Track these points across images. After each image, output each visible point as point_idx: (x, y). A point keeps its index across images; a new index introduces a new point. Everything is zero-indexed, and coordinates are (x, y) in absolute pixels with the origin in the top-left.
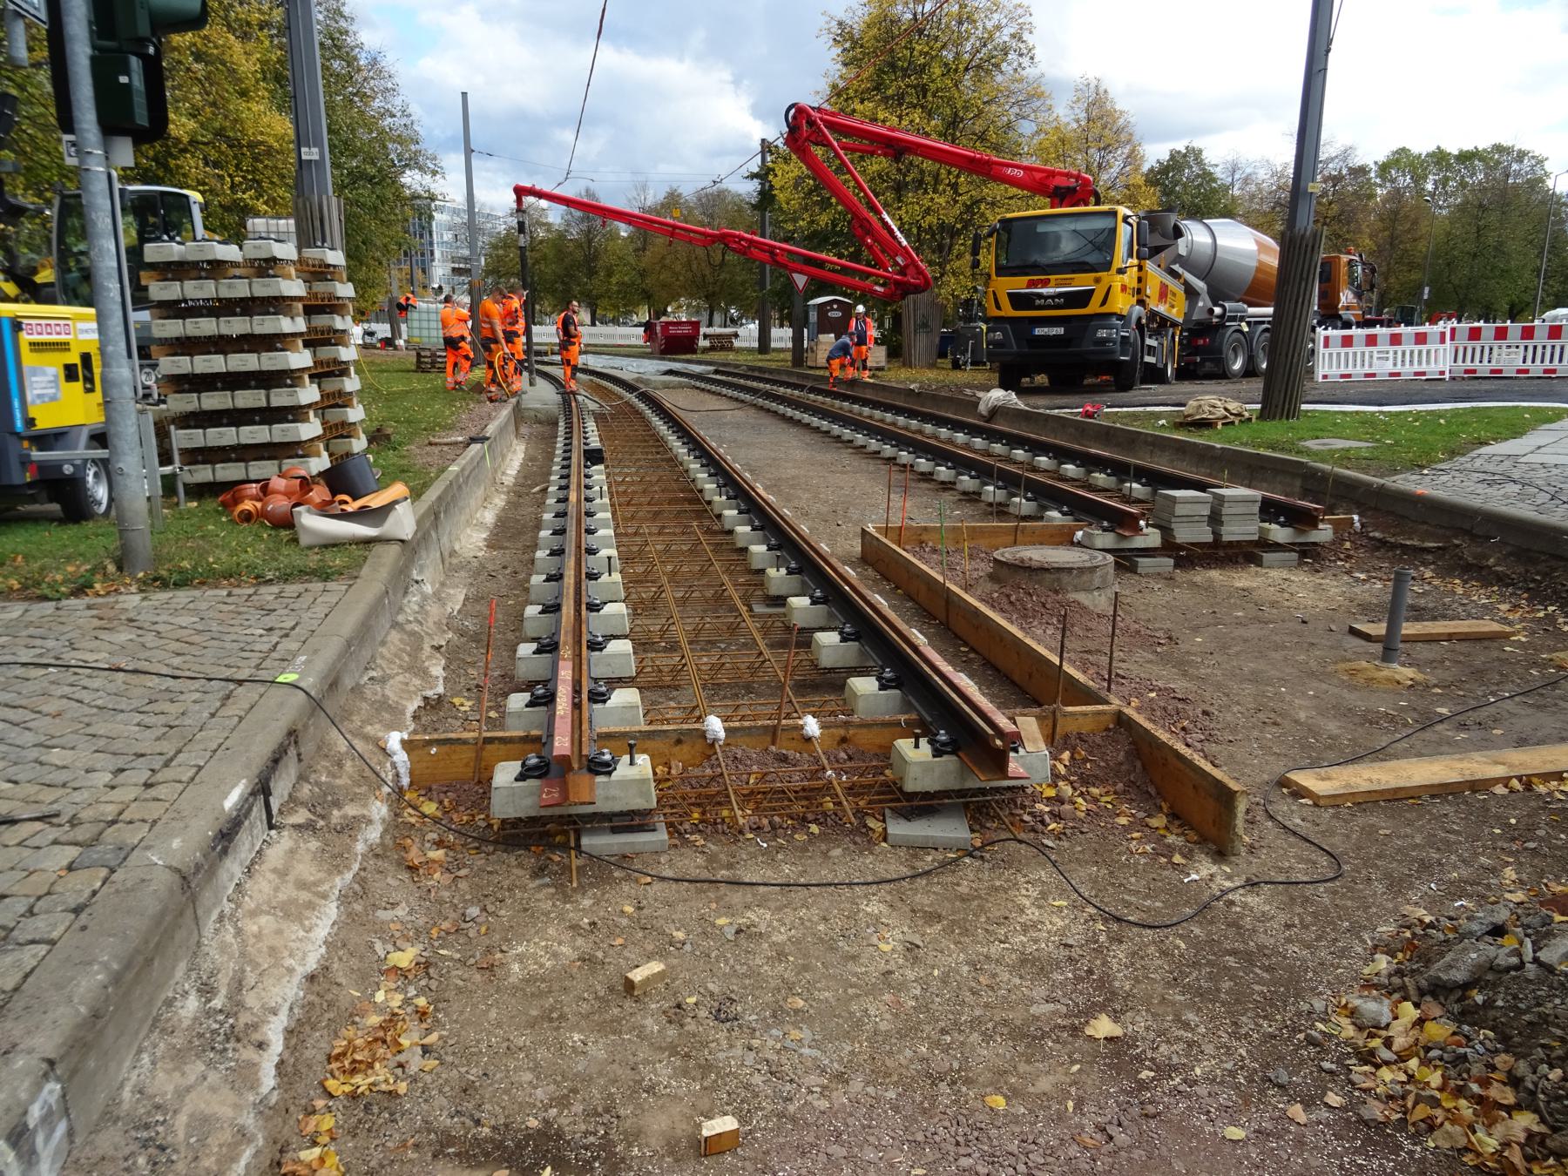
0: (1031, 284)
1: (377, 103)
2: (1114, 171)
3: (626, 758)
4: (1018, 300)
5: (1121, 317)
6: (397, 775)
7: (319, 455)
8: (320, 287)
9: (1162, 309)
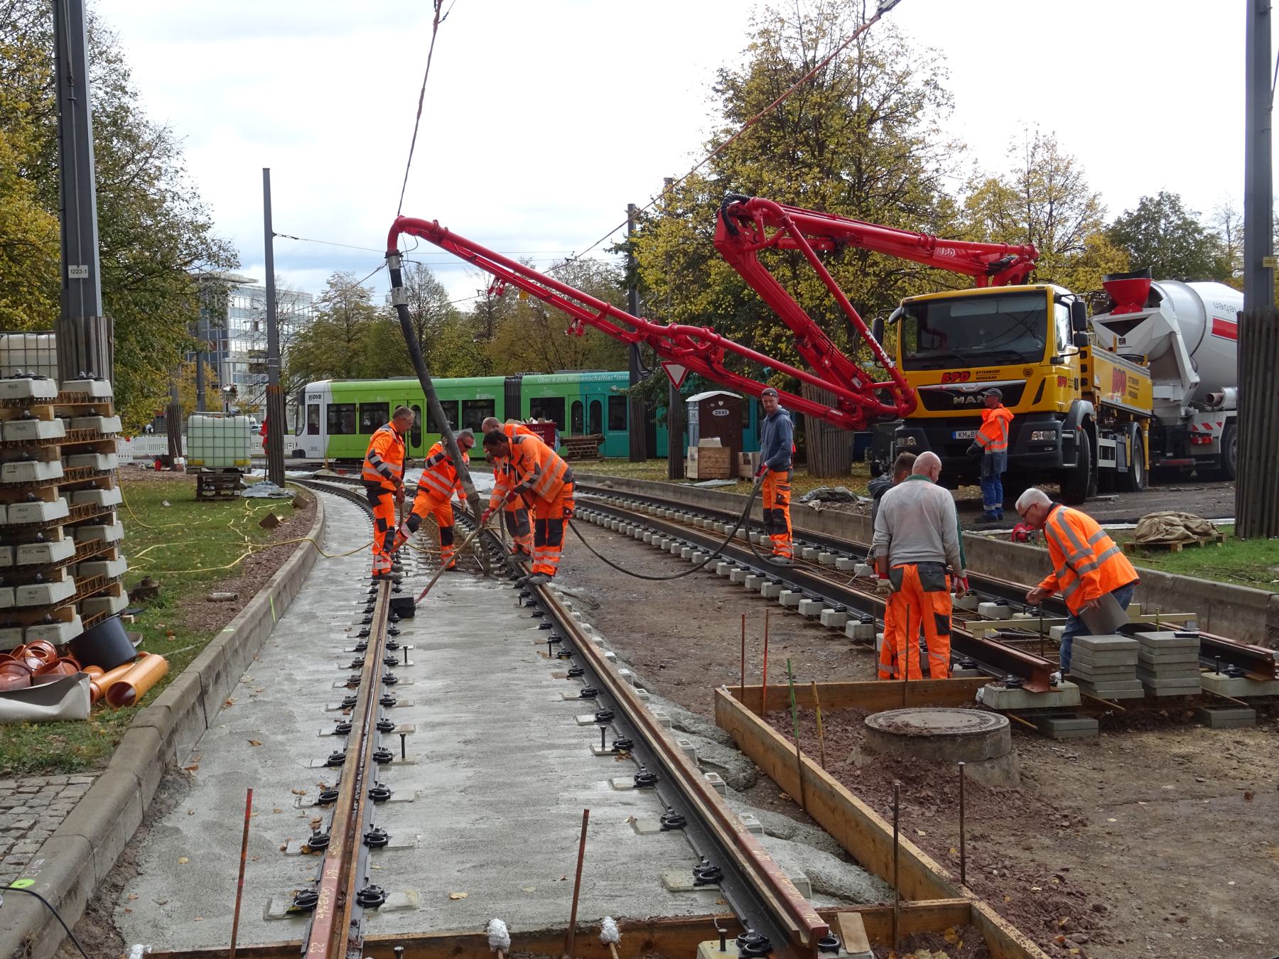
0: (948, 378)
2: (1071, 225)
4: (935, 399)
5: (1062, 416)
8: (82, 425)
9: (1117, 399)
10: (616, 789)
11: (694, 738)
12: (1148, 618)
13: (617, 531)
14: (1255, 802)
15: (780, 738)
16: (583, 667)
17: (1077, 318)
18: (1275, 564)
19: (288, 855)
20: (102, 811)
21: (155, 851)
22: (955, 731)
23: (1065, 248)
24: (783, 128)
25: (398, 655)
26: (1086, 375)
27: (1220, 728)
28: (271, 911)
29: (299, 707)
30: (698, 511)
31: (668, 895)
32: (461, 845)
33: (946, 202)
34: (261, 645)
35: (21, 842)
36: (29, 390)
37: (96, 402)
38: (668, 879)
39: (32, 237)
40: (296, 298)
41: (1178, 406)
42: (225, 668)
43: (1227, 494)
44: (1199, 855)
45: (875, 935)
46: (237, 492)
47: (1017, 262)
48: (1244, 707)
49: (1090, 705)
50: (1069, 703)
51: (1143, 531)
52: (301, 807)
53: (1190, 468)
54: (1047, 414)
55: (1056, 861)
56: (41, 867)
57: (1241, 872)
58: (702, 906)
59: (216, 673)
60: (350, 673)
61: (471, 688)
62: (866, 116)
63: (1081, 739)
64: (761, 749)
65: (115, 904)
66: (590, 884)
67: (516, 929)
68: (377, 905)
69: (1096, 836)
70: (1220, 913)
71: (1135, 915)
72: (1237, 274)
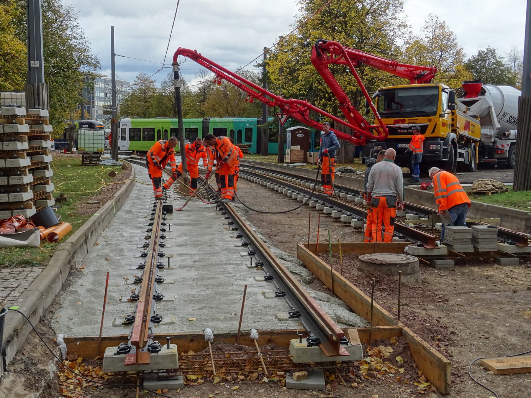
0: (396, 122)
1: (68, 32)
3: (166, 346)
5: (443, 139)
6: (61, 354)
7: (31, 208)
8: (36, 128)
9: (466, 133)
10: (256, 281)
11: (289, 263)
12: (476, 220)
13: (256, 183)
14: (518, 294)
15: (324, 263)
16: (243, 234)
17: (451, 99)
18: (529, 201)
19: (122, 302)
20: (46, 282)
21: (67, 299)
22: (396, 262)
23: (446, 71)
24: (330, 16)
25: (166, 227)
26: (454, 122)
27: (504, 265)
28: (116, 323)
29: (125, 246)
30: (290, 175)
31: (278, 322)
32: (193, 300)
33: (397, 50)
34: (110, 222)
35: (13, 292)
36: (14, 111)
37: (42, 119)
38: (278, 315)
39: (14, 52)
40: (123, 84)
41: (491, 137)
42: (95, 230)
43: (511, 174)
44: (494, 314)
45: (362, 339)
46: (98, 162)
47: (428, 74)
48: (514, 257)
49: (451, 255)
50: (443, 254)
51: (475, 187)
52: (127, 284)
53: (495, 163)
54: (436, 138)
55: (436, 314)
56: (22, 302)
57: (511, 320)
58: (292, 326)
59: (91, 231)
60: (146, 234)
61: (197, 241)
62: (365, 13)
63: (447, 268)
64: (316, 268)
65: (51, 319)
66: (246, 317)
67: (216, 333)
68: (159, 322)
69: (452, 306)
70: (502, 336)
71: (468, 336)
72: (517, 84)
